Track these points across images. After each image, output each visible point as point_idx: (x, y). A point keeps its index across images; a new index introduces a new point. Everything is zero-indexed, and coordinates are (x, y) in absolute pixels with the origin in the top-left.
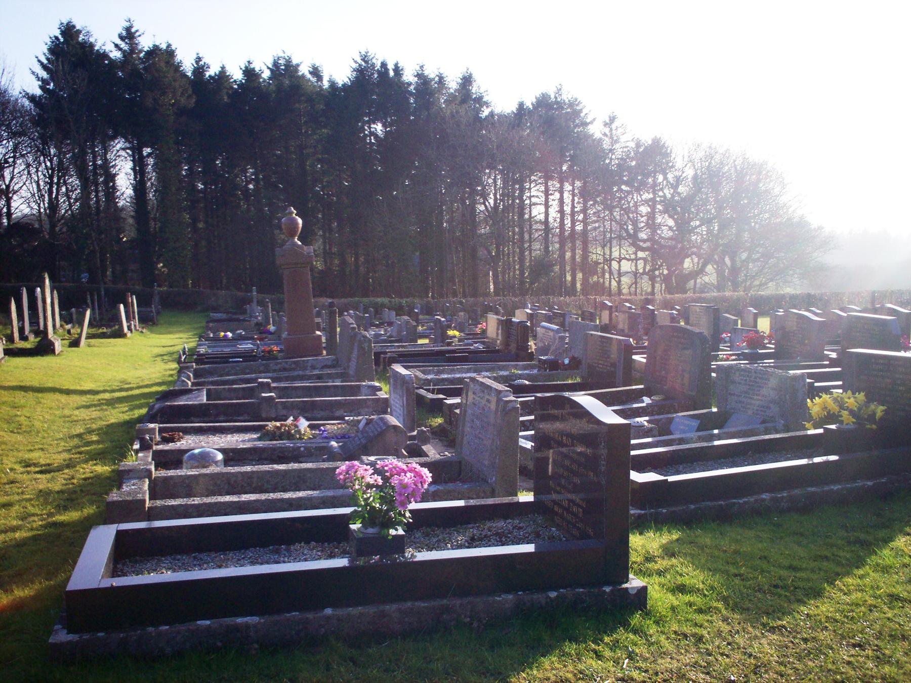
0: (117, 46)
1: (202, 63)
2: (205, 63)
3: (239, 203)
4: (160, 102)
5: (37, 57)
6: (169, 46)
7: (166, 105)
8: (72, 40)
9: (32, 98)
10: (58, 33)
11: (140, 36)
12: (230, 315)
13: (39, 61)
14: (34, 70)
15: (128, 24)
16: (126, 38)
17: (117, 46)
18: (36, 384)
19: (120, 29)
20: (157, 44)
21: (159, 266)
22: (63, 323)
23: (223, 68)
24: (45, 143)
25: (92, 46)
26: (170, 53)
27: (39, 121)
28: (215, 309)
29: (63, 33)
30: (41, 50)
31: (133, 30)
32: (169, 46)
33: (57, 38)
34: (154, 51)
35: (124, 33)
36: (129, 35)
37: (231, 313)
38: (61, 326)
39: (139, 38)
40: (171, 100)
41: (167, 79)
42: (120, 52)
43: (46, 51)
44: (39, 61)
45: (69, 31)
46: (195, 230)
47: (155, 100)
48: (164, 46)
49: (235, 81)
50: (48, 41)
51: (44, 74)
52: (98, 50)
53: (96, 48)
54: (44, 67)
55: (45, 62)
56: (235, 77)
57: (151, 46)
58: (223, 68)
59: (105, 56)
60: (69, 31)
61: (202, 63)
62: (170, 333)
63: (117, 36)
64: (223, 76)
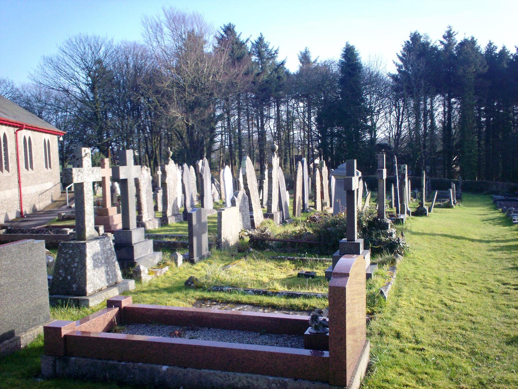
0: (441, 42)
1: (492, 46)
2: (494, 46)
3: (511, 128)
4: (467, 71)
5: (397, 54)
6: (473, 38)
7: (470, 73)
8: (418, 42)
9: (394, 77)
10: (409, 39)
11: (455, 35)
12: (507, 197)
13: (398, 56)
14: (395, 61)
15: (448, 29)
16: (447, 37)
17: (441, 42)
18: (458, 235)
19: (444, 32)
20: (466, 38)
21: (453, 166)
22: (412, 198)
23: (504, 48)
24: (397, 100)
25: (428, 44)
26: (473, 42)
27: (396, 89)
28: (496, 193)
29: (412, 39)
30: (399, 48)
31: (452, 32)
32: (473, 38)
33: (408, 42)
34: (463, 44)
35: (446, 35)
36: (449, 35)
37: (508, 195)
38: (411, 200)
39: (455, 37)
40: (473, 70)
41: (472, 58)
42: (443, 46)
43: (402, 50)
44: (398, 56)
45: (415, 38)
46: (479, 145)
47: (463, 70)
48: (470, 39)
49: (512, 55)
50: (404, 44)
51: (400, 63)
52: (432, 46)
53: (431, 45)
54: (401, 59)
55: (401, 56)
56: (511, 52)
57: (463, 40)
58: (504, 48)
59: (435, 48)
60: (415, 38)
61: (492, 46)
62: (474, 206)
63: (442, 37)
64: (503, 52)
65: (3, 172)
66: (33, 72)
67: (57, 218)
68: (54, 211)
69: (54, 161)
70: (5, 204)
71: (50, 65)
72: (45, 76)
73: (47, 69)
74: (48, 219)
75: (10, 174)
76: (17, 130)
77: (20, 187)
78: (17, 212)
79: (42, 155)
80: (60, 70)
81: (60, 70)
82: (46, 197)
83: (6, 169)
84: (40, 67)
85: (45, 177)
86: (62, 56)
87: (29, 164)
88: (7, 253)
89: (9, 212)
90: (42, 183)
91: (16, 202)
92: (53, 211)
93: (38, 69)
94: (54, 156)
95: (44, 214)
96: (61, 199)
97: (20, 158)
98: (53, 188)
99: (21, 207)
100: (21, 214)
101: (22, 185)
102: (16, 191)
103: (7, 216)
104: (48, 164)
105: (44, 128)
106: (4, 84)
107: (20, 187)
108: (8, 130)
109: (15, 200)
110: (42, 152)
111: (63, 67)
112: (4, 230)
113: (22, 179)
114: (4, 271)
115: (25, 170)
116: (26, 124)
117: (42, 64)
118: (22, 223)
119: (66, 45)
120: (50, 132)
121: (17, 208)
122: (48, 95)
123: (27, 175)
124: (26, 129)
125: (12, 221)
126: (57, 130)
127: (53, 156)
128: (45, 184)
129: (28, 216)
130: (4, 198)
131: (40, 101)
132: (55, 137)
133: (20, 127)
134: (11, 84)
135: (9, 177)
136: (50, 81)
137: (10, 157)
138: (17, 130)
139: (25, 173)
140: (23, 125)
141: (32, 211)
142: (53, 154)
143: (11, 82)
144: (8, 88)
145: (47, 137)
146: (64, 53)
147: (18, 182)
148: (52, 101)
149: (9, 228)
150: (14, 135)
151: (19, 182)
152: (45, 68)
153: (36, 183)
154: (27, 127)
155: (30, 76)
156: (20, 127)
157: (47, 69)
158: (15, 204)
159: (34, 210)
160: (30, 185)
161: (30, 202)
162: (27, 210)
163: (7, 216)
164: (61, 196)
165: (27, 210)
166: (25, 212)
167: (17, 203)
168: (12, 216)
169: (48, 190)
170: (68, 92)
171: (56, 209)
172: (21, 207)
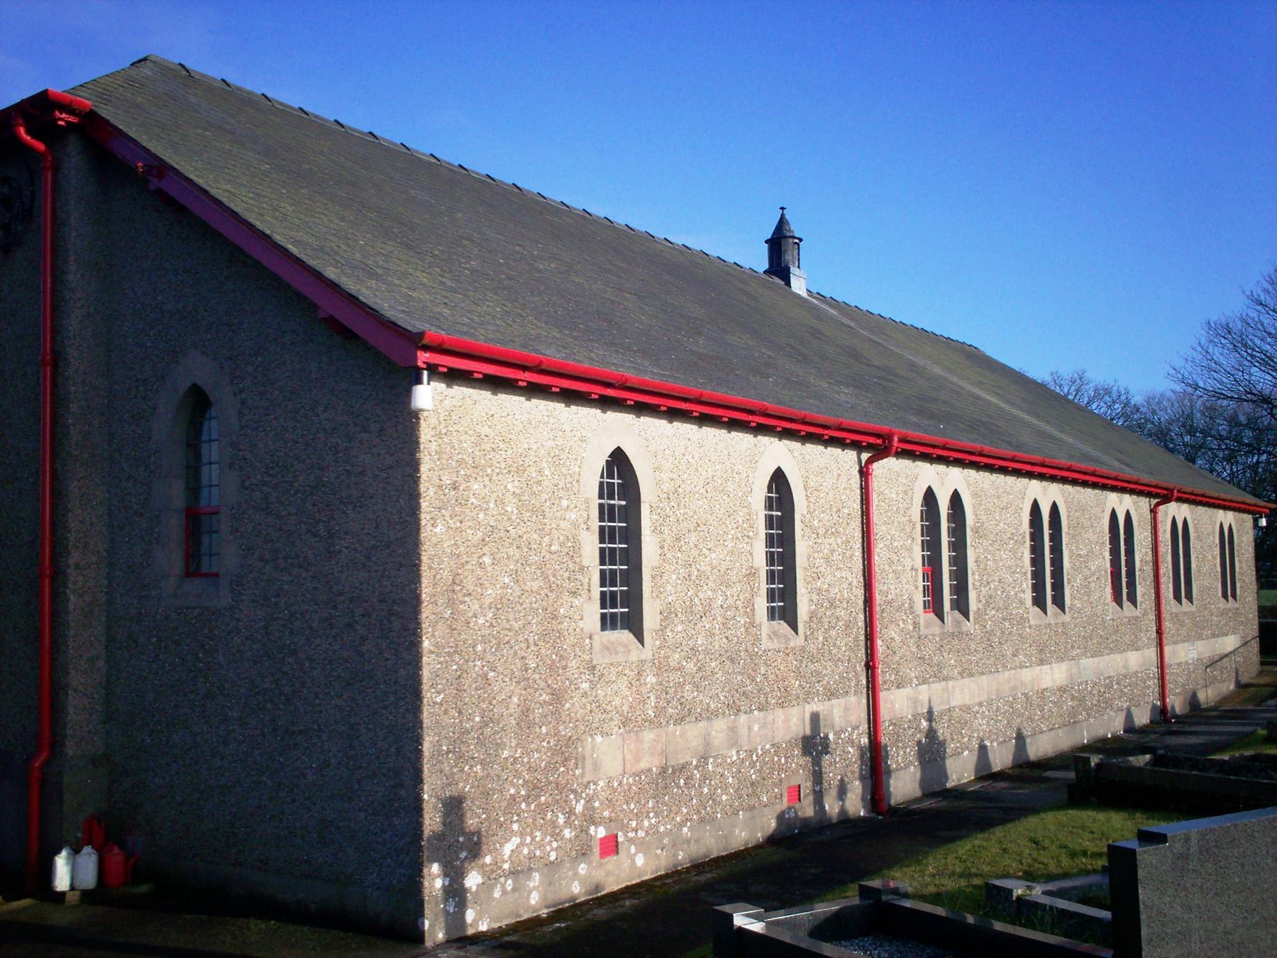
65: (1121, 607)
66: (1179, 363)
67: (1262, 732)
68: (1247, 711)
69: (1244, 581)
70: (1126, 687)
71: (1223, 341)
72: (1210, 369)
73: (1216, 352)
74: (1236, 733)
75: (1138, 613)
76: (1158, 504)
77: (1160, 645)
78: (1154, 706)
79: (1215, 565)
80: (1249, 351)
81: (1249, 351)
82: (1222, 673)
83: (1128, 599)
84: (1200, 349)
85: (1220, 621)
86: (1254, 315)
87: (1183, 589)
88: (1243, 842)
89: (1135, 706)
90: (1214, 636)
91: (1150, 683)
92: (1242, 711)
93: (1195, 354)
94: (1244, 566)
95: (1215, 717)
96: (1262, 681)
97: (1162, 571)
98: (1241, 650)
99: (1163, 696)
100: (1162, 713)
101: (1165, 641)
102: (1151, 653)
103: (1129, 716)
104: (1229, 588)
105: (1223, 496)
106: (1107, 398)
107: (1160, 645)
108: (1135, 503)
109: (1149, 678)
110: (1214, 558)
111: (1258, 342)
112: (1148, 757)
113: (1167, 625)
114: (1235, 892)
115: (1173, 602)
116: (1178, 487)
117: (1203, 341)
118: (1167, 737)
119: (1266, 285)
120: (1235, 505)
121: (1152, 697)
122: (1211, 412)
123: (1177, 614)
124: (1179, 500)
125: (1143, 730)
126: (1250, 499)
127: (1241, 568)
128: (1220, 640)
129: (1180, 719)
130: (1124, 671)
131: (1192, 431)
132: (1248, 518)
133: (1165, 496)
134: (1123, 398)
135: (1136, 618)
136: (1224, 380)
137: (1140, 570)
138: (1158, 504)
139: (1174, 610)
140: (1171, 491)
141: (1188, 707)
142: (1240, 562)
143: (1123, 392)
144: (1116, 406)
145: (1227, 518)
146: (1259, 308)
147: (1157, 632)
148: (1223, 428)
149: (1161, 752)
150: (1148, 516)
151: (1159, 632)
152: (1210, 350)
153: (1200, 638)
154: (1180, 495)
155: (1172, 372)
156: (1164, 495)
157: (1216, 352)
158: (1149, 687)
159: (1193, 702)
160: (1184, 641)
161: (1183, 685)
162: (1176, 703)
163: (1129, 716)
164: (1260, 674)
165: (1176, 703)
166: (1173, 708)
167: (1153, 683)
168: (1142, 718)
169: (1227, 655)
170: (1270, 403)
171: (1250, 707)
172: (1163, 696)
